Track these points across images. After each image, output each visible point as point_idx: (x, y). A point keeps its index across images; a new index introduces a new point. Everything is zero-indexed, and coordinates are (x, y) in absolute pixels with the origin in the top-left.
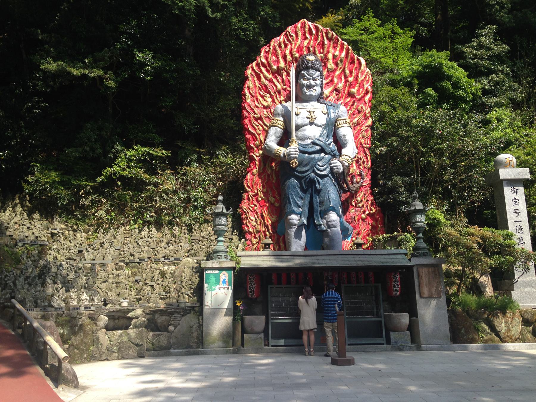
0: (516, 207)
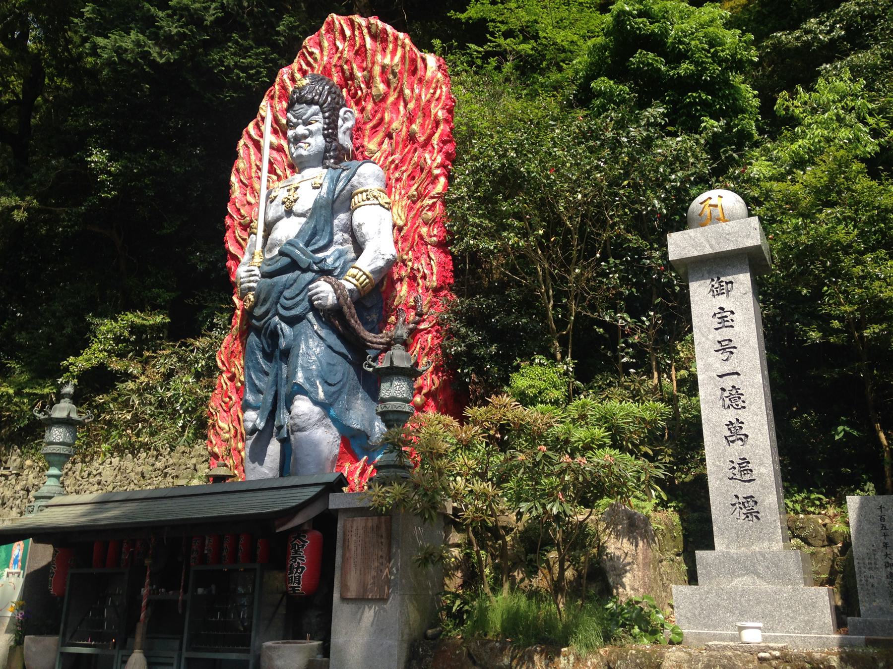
0: (726, 333)
